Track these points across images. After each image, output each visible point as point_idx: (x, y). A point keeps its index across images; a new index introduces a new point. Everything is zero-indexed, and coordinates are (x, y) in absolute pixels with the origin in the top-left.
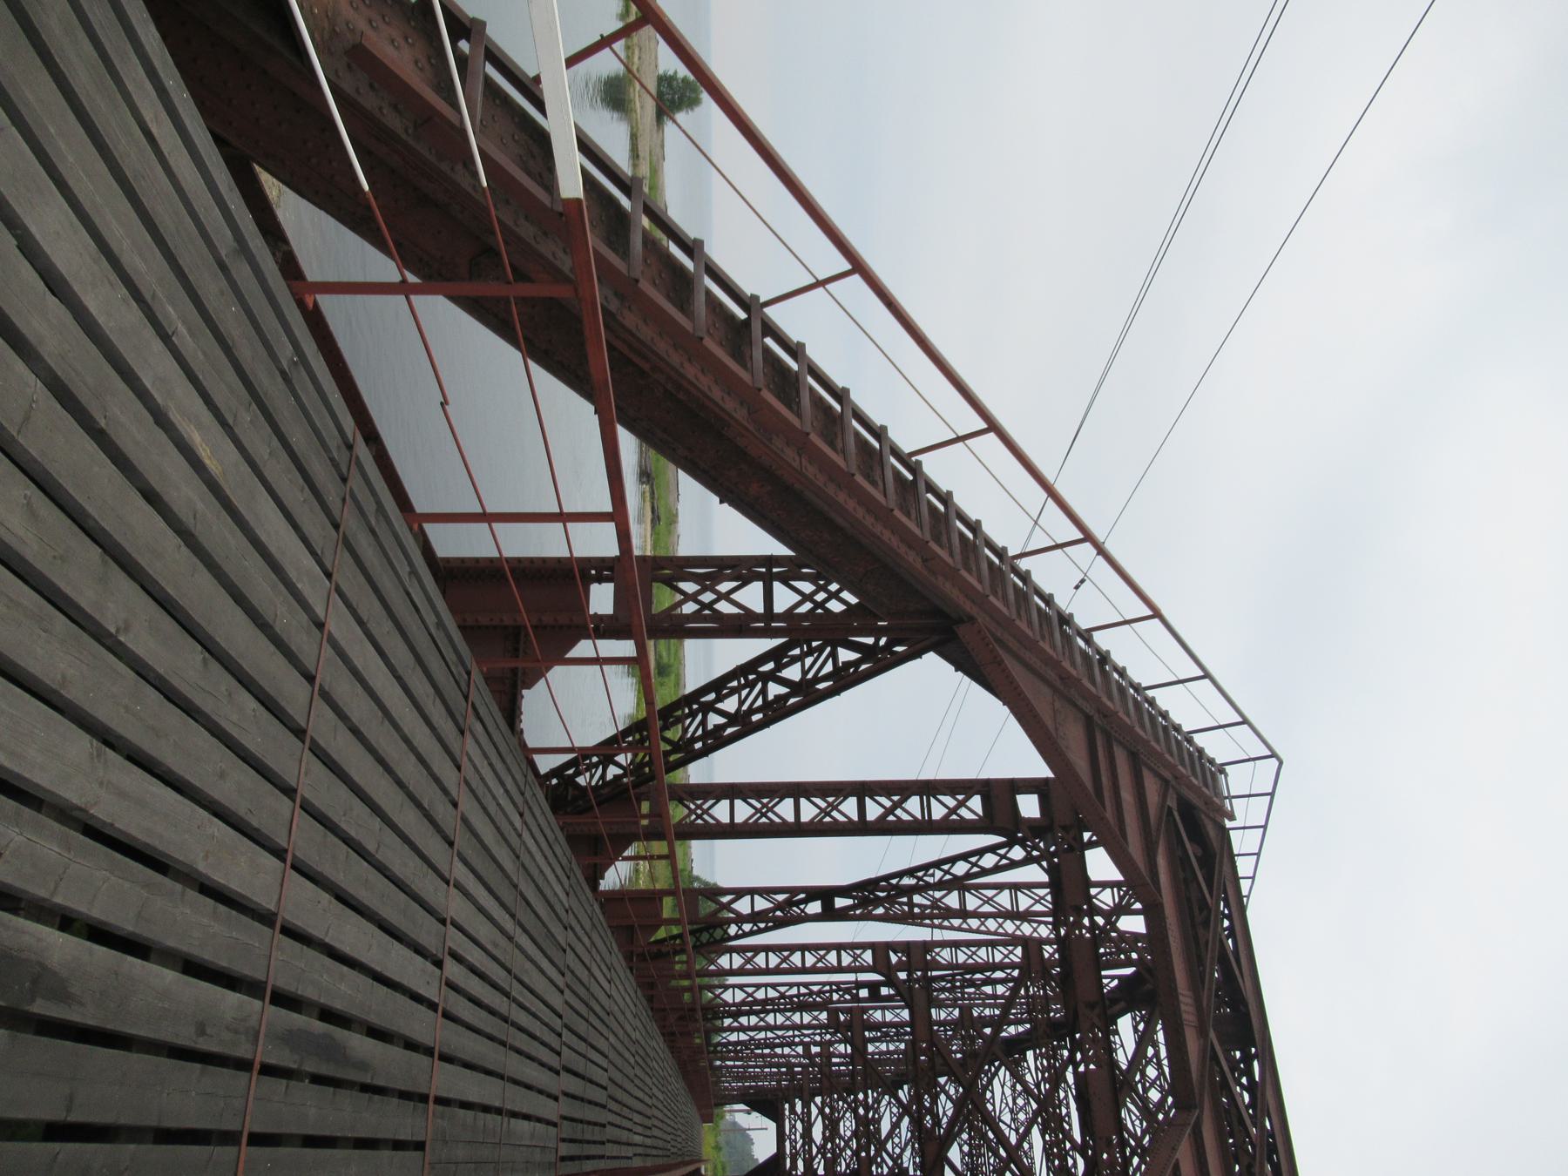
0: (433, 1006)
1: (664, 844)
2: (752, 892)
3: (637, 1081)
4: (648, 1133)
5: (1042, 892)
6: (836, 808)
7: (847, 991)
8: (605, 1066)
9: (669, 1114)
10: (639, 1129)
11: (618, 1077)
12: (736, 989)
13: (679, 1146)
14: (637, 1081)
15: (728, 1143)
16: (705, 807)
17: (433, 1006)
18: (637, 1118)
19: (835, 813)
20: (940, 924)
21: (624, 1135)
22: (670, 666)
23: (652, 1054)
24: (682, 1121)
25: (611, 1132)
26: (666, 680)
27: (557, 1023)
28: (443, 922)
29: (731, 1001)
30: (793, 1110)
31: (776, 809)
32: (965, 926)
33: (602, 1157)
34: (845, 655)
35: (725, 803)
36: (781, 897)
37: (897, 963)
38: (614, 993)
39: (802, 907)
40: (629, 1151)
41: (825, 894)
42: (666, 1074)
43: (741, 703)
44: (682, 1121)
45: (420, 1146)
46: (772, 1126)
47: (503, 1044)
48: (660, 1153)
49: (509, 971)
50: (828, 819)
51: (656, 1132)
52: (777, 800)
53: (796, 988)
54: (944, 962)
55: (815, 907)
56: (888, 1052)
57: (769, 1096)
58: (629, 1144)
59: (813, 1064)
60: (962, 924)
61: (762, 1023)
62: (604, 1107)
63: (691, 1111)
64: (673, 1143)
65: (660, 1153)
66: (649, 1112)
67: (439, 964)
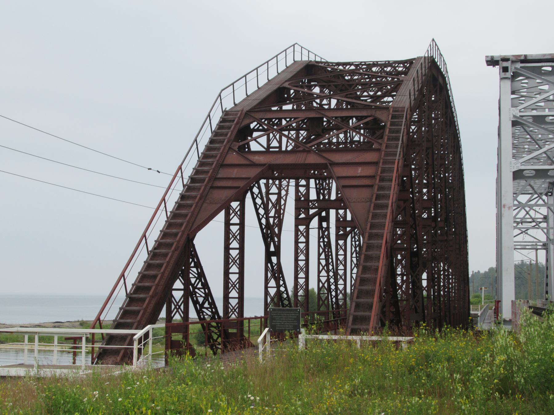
1: (245, 321)
2: (266, 287)
5: (271, 135)
6: (235, 210)
7: (323, 233)
12: (321, 275)
16: (232, 308)
19: (236, 210)
20: (283, 210)
29: (326, 278)
31: (234, 233)
32: (284, 198)
34: (192, 265)
35: (230, 300)
36: (269, 275)
37: (305, 214)
39: (274, 265)
41: (269, 255)
43: (201, 296)
50: (239, 213)
52: (230, 281)
53: (321, 261)
54: (305, 191)
55: (274, 259)
60: (283, 199)
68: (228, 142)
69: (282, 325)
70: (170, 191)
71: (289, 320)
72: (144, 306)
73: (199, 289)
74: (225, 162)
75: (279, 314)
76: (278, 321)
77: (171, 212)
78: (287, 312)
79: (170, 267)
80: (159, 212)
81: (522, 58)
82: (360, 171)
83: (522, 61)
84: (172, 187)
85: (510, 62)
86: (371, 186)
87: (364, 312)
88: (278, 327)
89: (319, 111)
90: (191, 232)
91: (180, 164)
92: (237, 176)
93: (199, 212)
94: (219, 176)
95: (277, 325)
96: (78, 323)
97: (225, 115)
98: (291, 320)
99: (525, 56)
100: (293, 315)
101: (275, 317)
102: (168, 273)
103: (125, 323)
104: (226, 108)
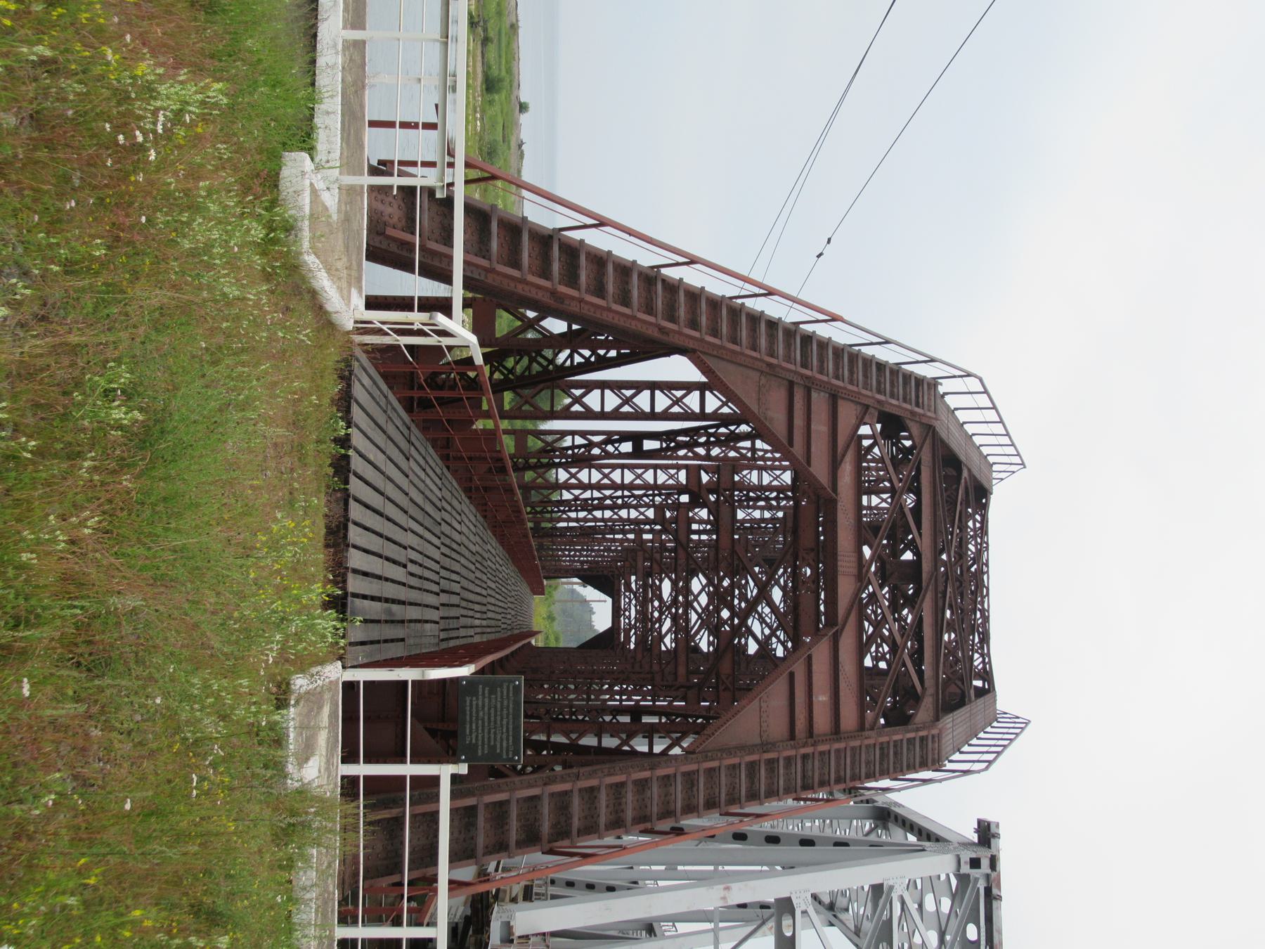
0: (404, 584)
3: (477, 582)
4: (485, 616)
8: (458, 580)
9: (500, 598)
10: (478, 615)
11: (465, 583)
13: (509, 622)
14: (477, 582)
15: (564, 612)
17: (404, 584)
18: (477, 607)
21: (469, 621)
22: (500, 80)
23: (486, 555)
24: (512, 600)
25: (463, 621)
26: (496, 97)
27: (436, 567)
28: (405, 548)
30: (628, 588)
33: (458, 638)
38: (465, 530)
39: (616, 445)
40: (471, 632)
42: (497, 566)
44: (512, 600)
45: (403, 640)
46: (609, 600)
47: (420, 589)
48: (493, 630)
49: (421, 553)
51: (490, 615)
56: (763, 520)
57: (605, 572)
58: (472, 627)
59: (665, 530)
61: (606, 481)
62: (458, 606)
63: (524, 588)
64: (503, 620)
65: (493, 630)
66: (484, 601)
67: (405, 566)
68: (879, 402)
69: (477, 712)
70: (790, 303)
71: (489, 733)
72: (531, 278)
73: (571, 356)
74: (840, 402)
75: (505, 703)
76: (487, 700)
77: (743, 304)
78: (511, 727)
79: (622, 323)
80: (740, 283)
81: (995, 891)
82: (822, 698)
83: (988, 891)
84: (795, 305)
85: (989, 871)
86: (792, 736)
87: (518, 816)
88: (471, 701)
89: (933, 581)
90: (699, 357)
91: (845, 318)
92: (813, 435)
93: (740, 365)
94: (814, 395)
95: (477, 699)
96: (514, 21)
97: (929, 384)
98: (489, 738)
99: (999, 898)
100: (505, 744)
101: (499, 694)
102: (610, 319)
103: (490, 233)
104: (941, 384)
